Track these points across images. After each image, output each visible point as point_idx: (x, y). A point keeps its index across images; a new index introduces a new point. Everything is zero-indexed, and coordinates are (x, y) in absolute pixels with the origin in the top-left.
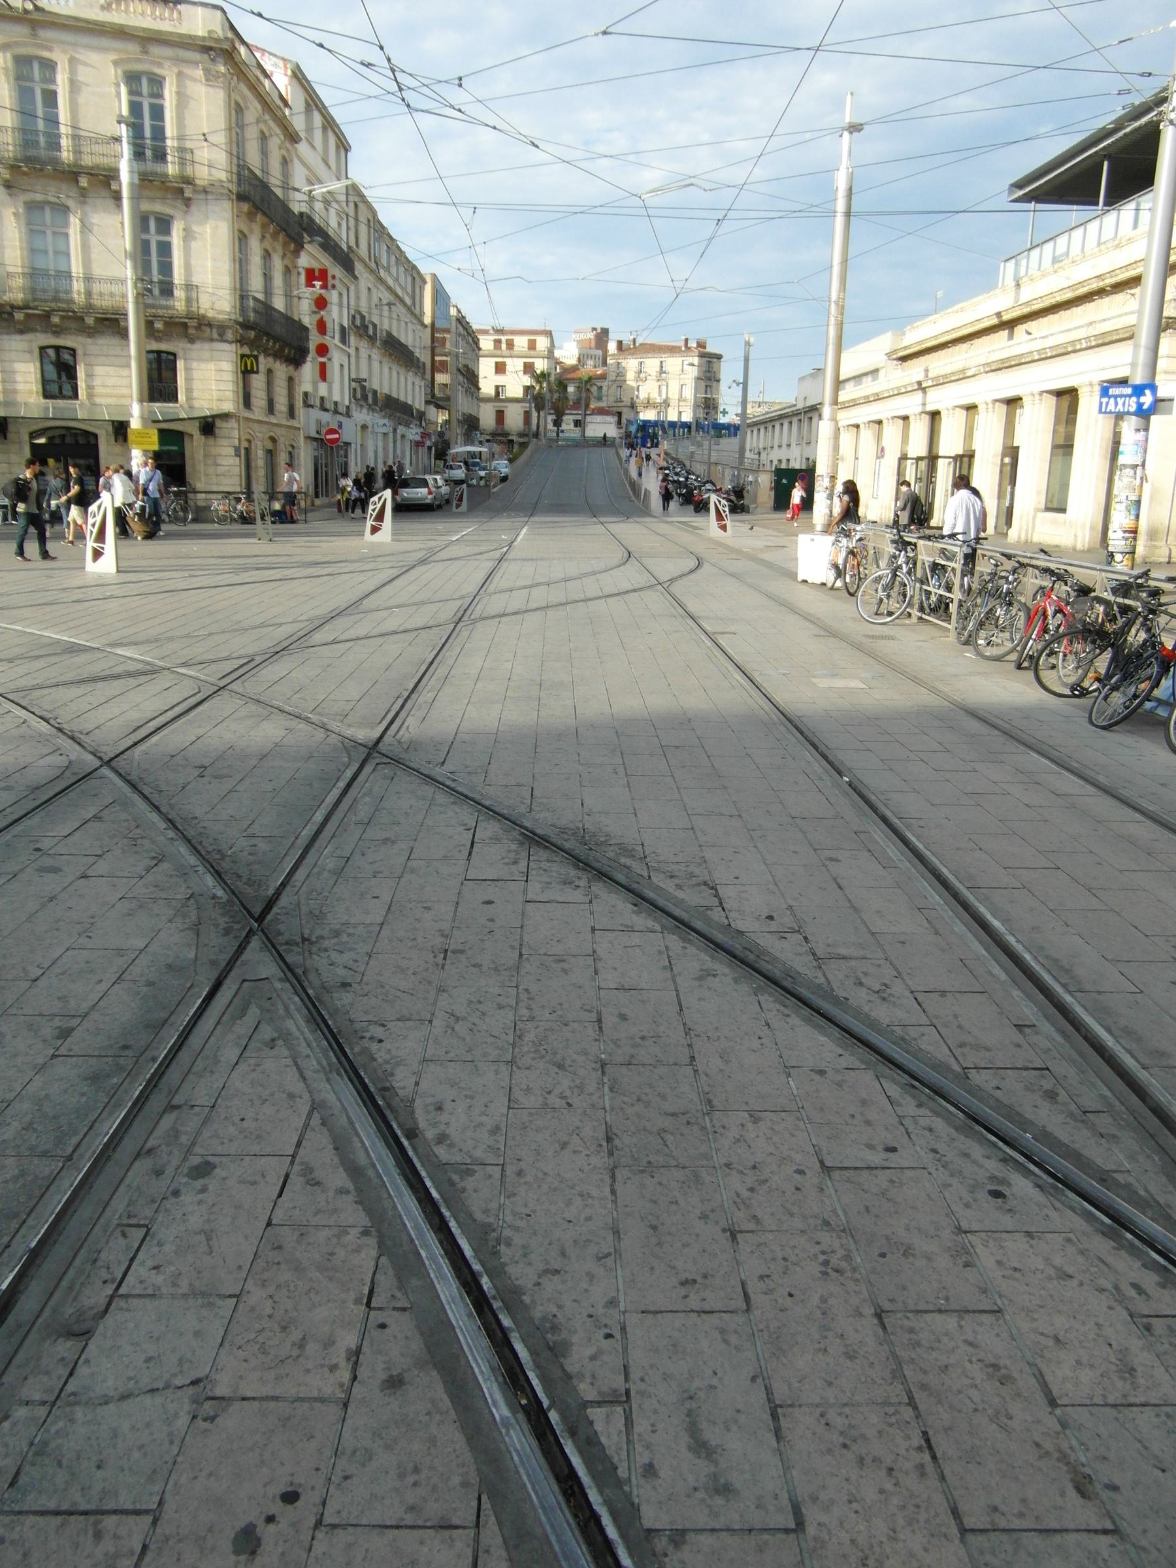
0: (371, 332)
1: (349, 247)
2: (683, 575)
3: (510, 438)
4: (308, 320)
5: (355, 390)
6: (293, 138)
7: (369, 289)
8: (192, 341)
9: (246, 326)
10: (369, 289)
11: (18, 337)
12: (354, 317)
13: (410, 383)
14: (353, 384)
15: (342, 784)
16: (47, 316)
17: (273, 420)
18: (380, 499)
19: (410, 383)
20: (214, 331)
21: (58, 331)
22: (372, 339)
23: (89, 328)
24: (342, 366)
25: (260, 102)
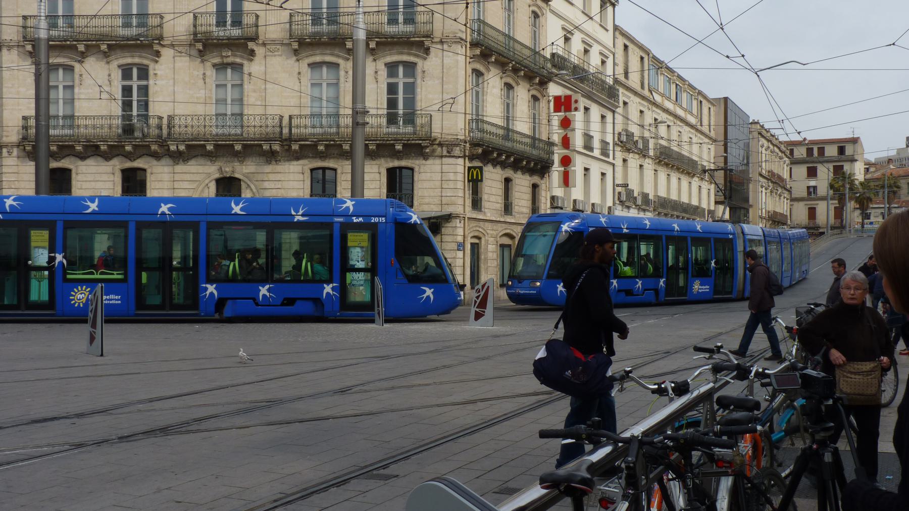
0: (640, 145)
1: (616, 81)
2: (414, 354)
3: (821, 230)
4: (556, 138)
5: (620, 193)
7: (641, 112)
8: (426, 157)
9: (474, 144)
10: (641, 112)
11: (295, 163)
12: (620, 134)
14: (619, 189)
16: (315, 146)
17: (509, 219)
20: (444, 148)
21: (322, 156)
22: (643, 154)
24: (603, 174)
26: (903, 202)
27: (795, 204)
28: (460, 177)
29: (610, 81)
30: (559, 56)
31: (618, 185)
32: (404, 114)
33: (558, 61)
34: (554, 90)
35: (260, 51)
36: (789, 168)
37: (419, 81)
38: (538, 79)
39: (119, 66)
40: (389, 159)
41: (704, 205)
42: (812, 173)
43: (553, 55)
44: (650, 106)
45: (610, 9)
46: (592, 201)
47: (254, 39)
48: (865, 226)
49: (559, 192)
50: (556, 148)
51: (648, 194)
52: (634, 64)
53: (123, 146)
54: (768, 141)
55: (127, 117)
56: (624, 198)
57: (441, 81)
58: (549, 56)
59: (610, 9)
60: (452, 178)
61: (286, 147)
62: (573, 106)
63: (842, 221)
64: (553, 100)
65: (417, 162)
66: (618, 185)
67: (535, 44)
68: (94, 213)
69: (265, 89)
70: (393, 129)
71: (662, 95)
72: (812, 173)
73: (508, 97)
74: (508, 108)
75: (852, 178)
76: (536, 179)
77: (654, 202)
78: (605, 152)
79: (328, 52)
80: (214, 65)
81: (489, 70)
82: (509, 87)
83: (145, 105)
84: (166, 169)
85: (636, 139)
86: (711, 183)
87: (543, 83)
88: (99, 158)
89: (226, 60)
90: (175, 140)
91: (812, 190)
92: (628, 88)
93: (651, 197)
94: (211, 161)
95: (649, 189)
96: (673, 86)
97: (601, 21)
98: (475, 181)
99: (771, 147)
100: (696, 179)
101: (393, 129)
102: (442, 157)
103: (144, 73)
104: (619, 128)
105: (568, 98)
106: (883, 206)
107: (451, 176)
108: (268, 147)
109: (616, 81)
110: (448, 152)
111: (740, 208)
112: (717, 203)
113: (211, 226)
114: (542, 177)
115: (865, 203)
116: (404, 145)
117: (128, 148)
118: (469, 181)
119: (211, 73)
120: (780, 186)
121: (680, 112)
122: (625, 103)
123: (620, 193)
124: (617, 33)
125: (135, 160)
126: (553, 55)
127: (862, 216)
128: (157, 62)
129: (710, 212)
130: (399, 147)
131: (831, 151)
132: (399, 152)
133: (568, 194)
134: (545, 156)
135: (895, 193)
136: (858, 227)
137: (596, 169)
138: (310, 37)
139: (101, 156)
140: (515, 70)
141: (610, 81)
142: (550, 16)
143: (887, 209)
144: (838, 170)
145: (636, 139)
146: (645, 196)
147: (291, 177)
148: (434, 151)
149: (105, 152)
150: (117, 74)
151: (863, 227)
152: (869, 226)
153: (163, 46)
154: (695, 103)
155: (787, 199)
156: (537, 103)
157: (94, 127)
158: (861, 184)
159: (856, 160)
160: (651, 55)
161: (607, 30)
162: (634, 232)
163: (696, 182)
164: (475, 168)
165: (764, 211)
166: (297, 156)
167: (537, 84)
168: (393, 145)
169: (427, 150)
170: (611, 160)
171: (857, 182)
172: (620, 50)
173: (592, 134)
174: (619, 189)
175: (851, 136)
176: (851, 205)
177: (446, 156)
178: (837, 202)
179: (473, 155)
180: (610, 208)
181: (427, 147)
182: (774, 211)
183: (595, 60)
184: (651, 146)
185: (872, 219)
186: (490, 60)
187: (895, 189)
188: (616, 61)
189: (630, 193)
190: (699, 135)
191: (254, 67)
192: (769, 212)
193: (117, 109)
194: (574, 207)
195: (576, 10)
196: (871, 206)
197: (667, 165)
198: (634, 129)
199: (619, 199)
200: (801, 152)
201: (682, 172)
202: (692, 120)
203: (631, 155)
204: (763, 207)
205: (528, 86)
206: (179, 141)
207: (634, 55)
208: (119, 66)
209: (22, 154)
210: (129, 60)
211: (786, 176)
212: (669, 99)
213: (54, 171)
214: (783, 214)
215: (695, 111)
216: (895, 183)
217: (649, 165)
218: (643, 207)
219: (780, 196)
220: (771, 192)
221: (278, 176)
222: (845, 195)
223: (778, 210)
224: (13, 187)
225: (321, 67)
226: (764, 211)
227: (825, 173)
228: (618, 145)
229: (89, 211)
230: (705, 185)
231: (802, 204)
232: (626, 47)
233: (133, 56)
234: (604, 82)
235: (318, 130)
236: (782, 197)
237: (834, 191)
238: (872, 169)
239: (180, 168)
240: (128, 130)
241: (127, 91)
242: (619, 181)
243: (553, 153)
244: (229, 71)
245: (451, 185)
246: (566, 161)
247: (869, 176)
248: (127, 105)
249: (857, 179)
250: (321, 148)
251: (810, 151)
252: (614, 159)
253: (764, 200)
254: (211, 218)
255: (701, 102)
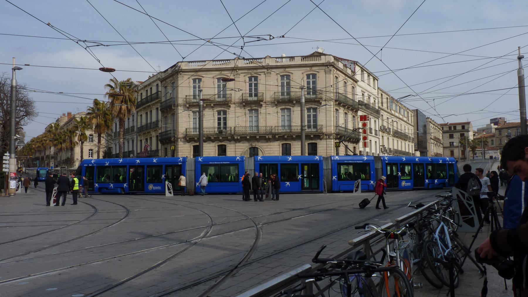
0: (388, 131)
1: (379, 107)
5: (381, 149)
6: (356, 81)
8: (321, 139)
9: (337, 135)
11: (277, 142)
12: (381, 127)
13: (433, 146)
14: (381, 147)
15: (20, 277)
16: (284, 136)
18: (357, 182)
19: (433, 146)
20: (327, 136)
21: (286, 140)
22: (389, 133)
23: (294, 138)
24: (376, 142)
25: (344, 75)
26: (490, 148)
27: (445, 149)
28: (333, 146)
29: (377, 108)
30: (361, 101)
31: (381, 146)
32: (313, 125)
33: (361, 103)
34: (360, 113)
35: (264, 105)
36: (442, 135)
37: (318, 114)
38: (355, 110)
39: (217, 111)
40: (308, 140)
41: (411, 152)
42: (451, 137)
43: (359, 101)
44: (390, 115)
45: (376, 81)
46: (373, 152)
47: (262, 101)
48: (475, 158)
49: (362, 149)
50: (361, 134)
51: (391, 148)
52: (385, 100)
53: (219, 137)
54: (434, 125)
55: (219, 128)
56: (383, 150)
57: (325, 113)
58: (358, 102)
59: (376, 81)
60: (330, 146)
61: (274, 137)
62: (367, 119)
63: (465, 156)
64: (359, 117)
65: (318, 141)
66: (381, 146)
67: (353, 98)
68: (290, 161)
69: (266, 117)
70: (310, 130)
71: (395, 111)
72: (451, 137)
73: (345, 117)
74: (346, 121)
75: (468, 139)
76: (355, 145)
77: (393, 151)
78: (376, 134)
79: (287, 105)
80: (248, 110)
81: (340, 109)
82: (346, 113)
83: (225, 124)
84: (233, 145)
85: (386, 128)
86: (413, 143)
87: (357, 111)
88: (210, 141)
89: (252, 108)
90: (237, 135)
91: (452, 143)
92: (383, 110)
93: (392, 150)
94: (248, 142)
95: (391, 147)
96: (398, 107)
97: (362, 79)
98: (337, 146)
99: (435, 127)
100: (407, 142)
101: (310, 130)
102: (326, 139)
103: (225, 113)
104: (380, 125)
105: (365, 116)
106: (481, 149)
107: (330, 146)
108: (268, 137)
109: (379, 107)
110: (329, 137)
111: (425, 152)
112: (415, 150)
113: (148, 166)
114: (357, 144)
115: (474, 149)
116: (314, 136)
117: (221, 138)
118: (335, 147)
119: (248, 112)
120: (439, 142)
121: (401, 117)
122: (382, 115)
123: (381, 149)
124: (379, 90)
125: (222, 142)
126: (359, 101)
127: (473, 154)
128: (229, 109)
129: (413, 154)
130: (312, 136)
131: (459, 128)
132: (312, 138)
133: (365, 150)
134: (357, 137)
135: (486, 144)
136: (471, 158)
137: (373, 140)
138: (281, 100)
139: (211, 141)
140: (348, 108)
141: (377, 108)
142: (357, 87)
143: (483, 151)
144: (462, 135)
145: (386, 128)
146: (390, 149)
147: (275, 147)
148: (323, 137)
149: (213, 139)
150: (216, 114)
151: (474, 158)
152: (476, 158)
153: (232, 104)
154: (406, 112)
155: (442, 148)
156: (346, 115)
157: (209, 132)
158: (472, 141)
159: (470, 131)
160: (390, 97)
161: (375, 89)
162: (390, 162)
163: (407, 143)
164: (337, 142)
165: (433, 153)
166: (277, 140)
167: (354, 112)
168: (310, 135)
169: (322, 137)
170: (378, 137)
171: (470, 140)
172: (380, 96)
173: (372, 127)
174: (381, 147)
175: (467, 121)
176: (468, 149)
177: (328, 139)
178: (462, 148)
179: (336, 138)
180: (378, 154)
181: (322, 136)
182: (437, 153)
183: (372, 101)
184: (391, 130)
185: (477, 155)
186: (349, 109)
187: (486, 143)
188: (379, 100)
189: (385, 148)
190: (408, 125)
191: (262, 110)
192: (435, 153)
193: (216, 125)
194: (367, 154)
195: (366, 84)
196: (477, 149)
197: (397, 137)
198: (385, 124)
199: (381, 151)
200: (446, 129)
201: (399, 138)
202: (405, 119)
203: (385, 134)
204: (433, 151)
205: (343, 109)
206: (237, 135)
207: (385, 96)
208: (217, 111)
209: (185, 141)
210: (220, 109)
211: (441, 138)
212: (397, 112)
213: (365, 142)
214: (440, 154)
215: (406, 116)
216: (486, 140)
217: (391, 138)
218: (389, 153)
219: (439, 146)
220: (435, 145)
221: (272, 147)
222: (466, 146)
223: (438, 152)
224: (182, 152)
225: (285, 110)
226: (433, 153)
227: (457, 135)
228: (380, 131)
229: (289, 160)
230: (411, 144)
231: (448, 149)
232: (382, 95)
233: (221, 107)
234: (375, 109)
235: (284, 131)
236: (440, 147)
237: (461, 144)
238: (476, 134)
239: (237, 144)
240: (220, 132)
241: (219, 119)
242: (381, 144)
243: (360, 136)
244: (253, 111)
245: (330, 148)
246: (365, 138)
247: (475, 137)
248: (219, 124)
249: (470, 139)
250: (286, 137)
251: (450, 128)
252: (379, 136)
253: (433, 148)
254: (302, 162)
255: (408, 112)
